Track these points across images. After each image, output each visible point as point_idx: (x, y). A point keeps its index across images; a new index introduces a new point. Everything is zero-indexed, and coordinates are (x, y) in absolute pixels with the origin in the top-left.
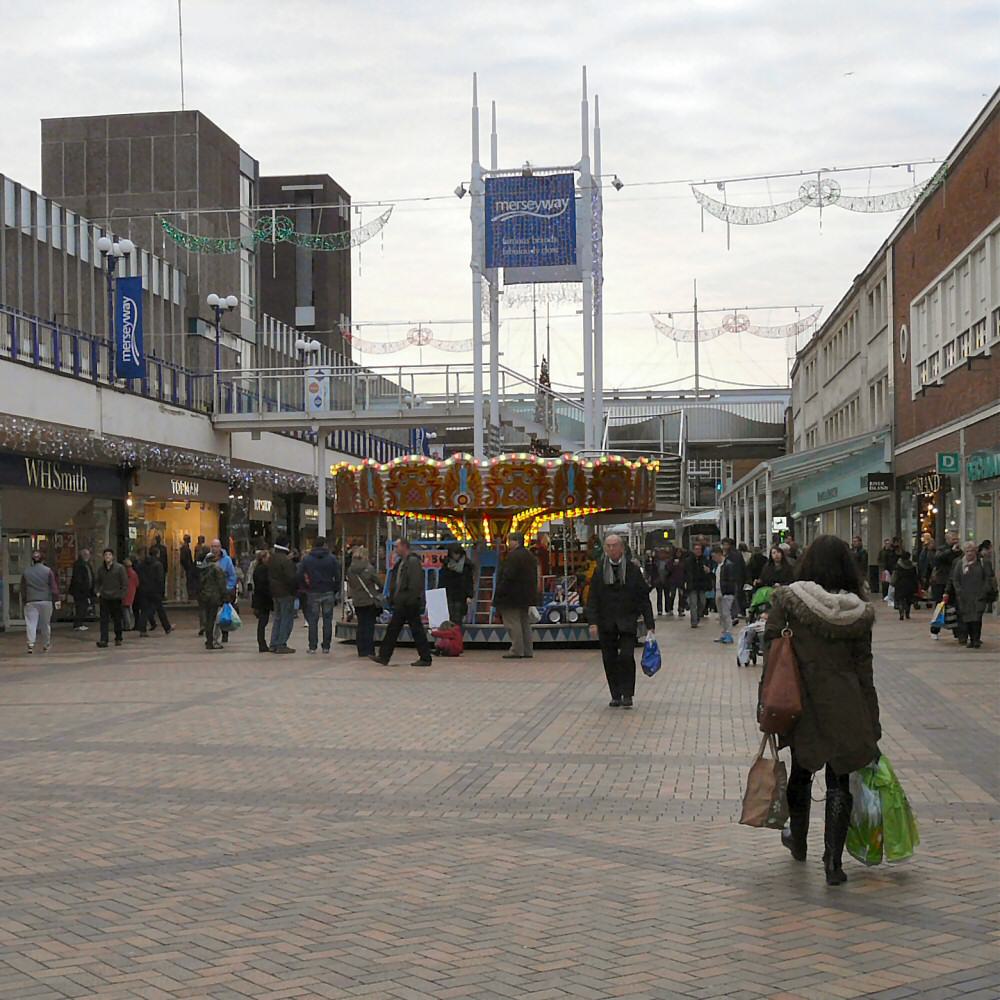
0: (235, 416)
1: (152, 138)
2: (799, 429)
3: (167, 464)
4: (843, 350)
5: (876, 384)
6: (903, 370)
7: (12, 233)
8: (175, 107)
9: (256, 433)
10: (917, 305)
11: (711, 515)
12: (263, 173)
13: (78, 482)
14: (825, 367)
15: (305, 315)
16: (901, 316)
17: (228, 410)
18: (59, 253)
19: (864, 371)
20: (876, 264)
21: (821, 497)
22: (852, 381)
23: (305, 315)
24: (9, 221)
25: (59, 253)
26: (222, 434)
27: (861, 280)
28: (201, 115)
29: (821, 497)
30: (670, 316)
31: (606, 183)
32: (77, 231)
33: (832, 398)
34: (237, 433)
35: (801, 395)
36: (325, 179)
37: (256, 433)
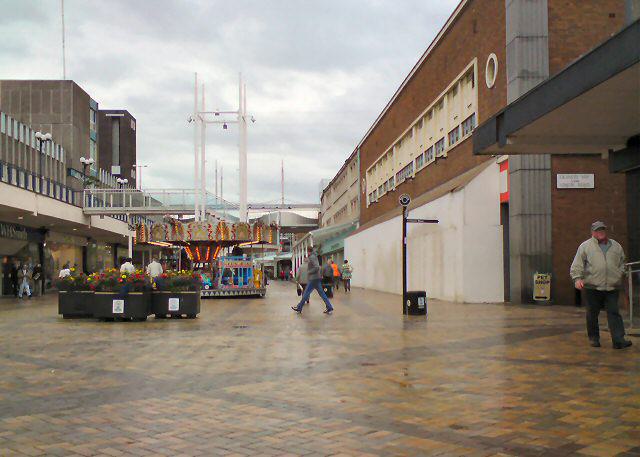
0: (92, 208)
1: (52, 91)
2: (324, 221)
3: (64, 226)
4: (341, 188)
5: (354, 201)
6: (363, 197)
7: (4, 135)
8: (57, 76)
9: (102, 216)
10: (370, 171)
11: (288, 256)
12: (100, 108)
13: (22, 235)
14: (334, 195)
15: (116, 170)
16: (363, 176)
17: (90, 206)
18: (10, 138)
19: (349, 197)
20: (354, 155)
21: (333, 247)
22: (345, 201)
23: (116, 170)
24: (3, 131)
25: (10, 138)
26: (87, 216)
27: (348, 162)
28: (75, 86)
29: (333, 247)
30: (225, 127)
31: (248, 120)
32: (19, 128)
33: (337, 208)
34: (499, 301)
35: (325, 207)
36: (125, 112)
37: (102, 216)
